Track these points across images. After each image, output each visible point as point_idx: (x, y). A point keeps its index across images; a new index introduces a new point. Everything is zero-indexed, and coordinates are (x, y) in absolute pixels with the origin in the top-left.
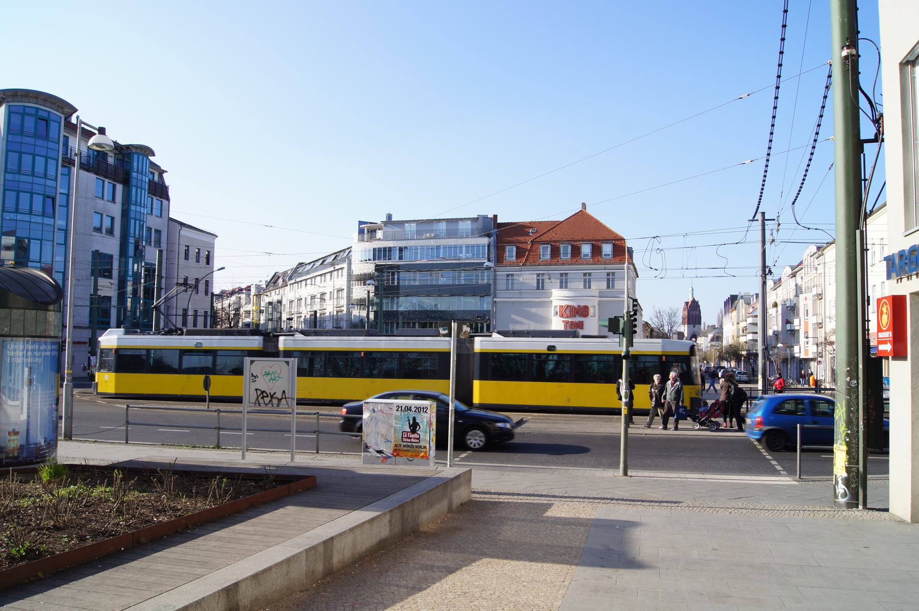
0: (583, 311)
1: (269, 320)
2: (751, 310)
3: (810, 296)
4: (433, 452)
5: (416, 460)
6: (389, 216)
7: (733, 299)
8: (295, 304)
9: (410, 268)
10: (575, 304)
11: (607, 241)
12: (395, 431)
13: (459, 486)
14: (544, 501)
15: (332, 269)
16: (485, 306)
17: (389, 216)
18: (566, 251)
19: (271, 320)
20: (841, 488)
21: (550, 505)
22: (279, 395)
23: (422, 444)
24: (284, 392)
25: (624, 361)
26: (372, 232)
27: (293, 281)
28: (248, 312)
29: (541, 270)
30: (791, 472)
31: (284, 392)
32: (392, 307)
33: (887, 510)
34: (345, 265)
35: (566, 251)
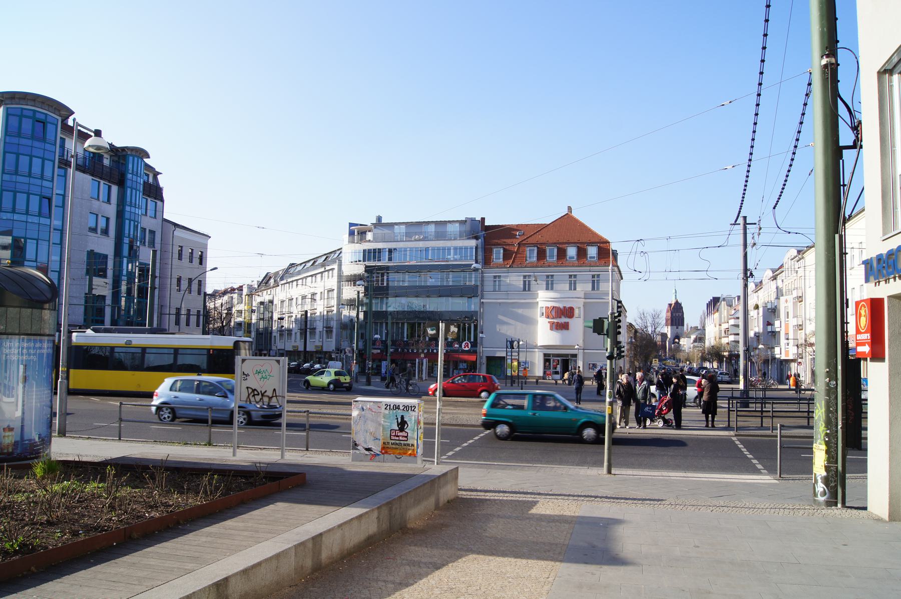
0: (568, 312)
1: (261, 319)
2: (733, 312)
3: (790, 298)
4: (420, 451)
5: (404, 457)
6: (379, 219)
7: (715, 301)
8: (286, 304)
9: (399, 269)
10: (561, 306)
11: (591, 244)
14: (529, 498)
15: (323, 270)
16: (473, 307)
17: (379, 219)
18: (552, 253)
19: (263, 319)
20: (820, 487)
22: (270, 393)
23: (410, 442)
24: (274, 390)
26: (362, 233)
28: (240, 312)
29: (528, 271)
30: (771, 470)
31: (274, 390)
33: (865, 508)
34: (335, 266)
35: (552, 253)
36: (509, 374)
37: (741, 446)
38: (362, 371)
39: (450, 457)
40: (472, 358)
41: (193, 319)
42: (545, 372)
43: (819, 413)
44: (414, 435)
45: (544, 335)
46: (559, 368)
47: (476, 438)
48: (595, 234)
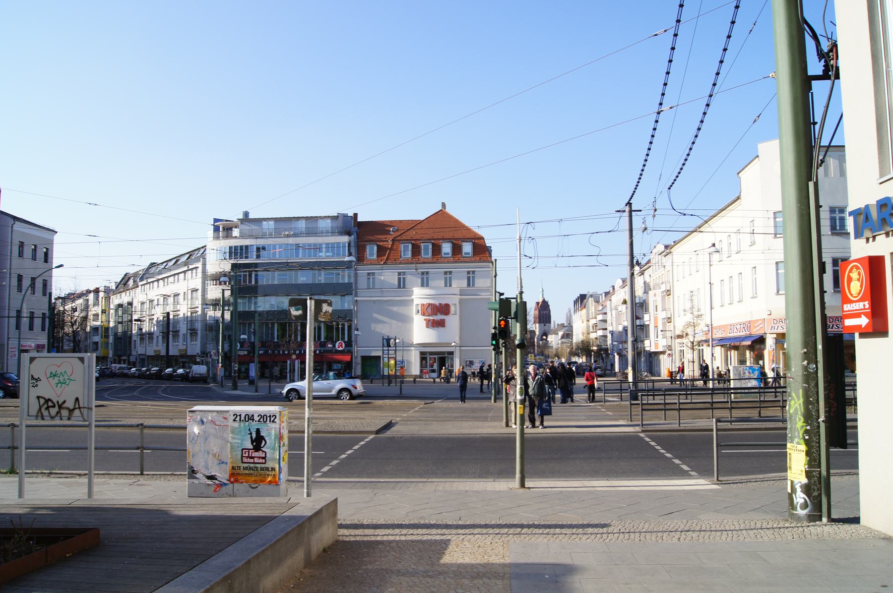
0: (444, 309)
1: (119, 323)
2: (601, 308)
3: (659, 292)
4: (284, 476)
5: (262, 487)
6: (246, 214)
7: (583, 297)
8: (147, 306)
9: (268, 267)
10: (437, 302)
11: (466, 240)
12: (232, 447)
13: (321, 524)
14: (435, 535)
15: (186, 268)
16: (346, 305)
17: (246, 214)
18: (427, 251)
19: (121, 323)
20: (800, 498)
21: (445, 544)
22: (70, 404)
23: (269, 464)
24: (77, 399)
25: (518, 350)
26: (228, 229)
27: (145, 282)
28: (96, 315)
29: (402, 268)
30: (704, 472)
31: (77, 399)
32: (250, 307)
33: (856, 520)
34: (200, 265)
35: (427, 251)
36: (386, 373)
37: (653, 443)
38: (228, 376)
39: (325, 475)
40: (347, 358)
41: (38, 322)
42: (421, 371)
43: (795, 404)
44: (275, 454)
45: (420, 333)
46: (435, 367)
47: (356, 447)
48: (468, 229)
